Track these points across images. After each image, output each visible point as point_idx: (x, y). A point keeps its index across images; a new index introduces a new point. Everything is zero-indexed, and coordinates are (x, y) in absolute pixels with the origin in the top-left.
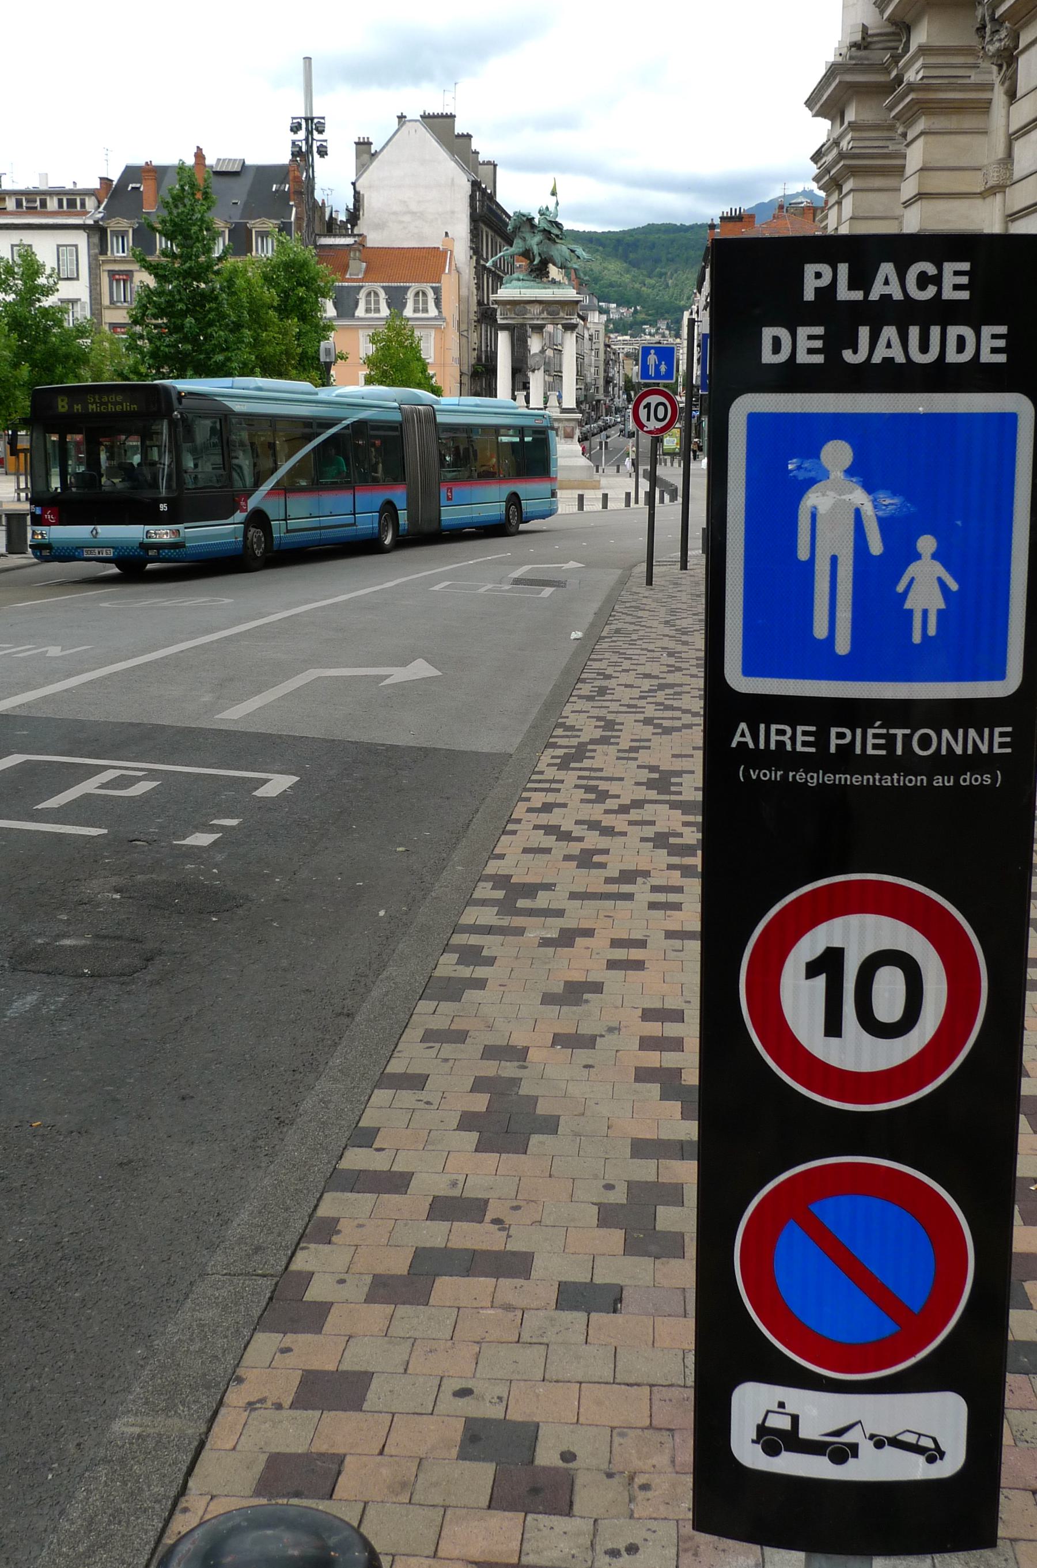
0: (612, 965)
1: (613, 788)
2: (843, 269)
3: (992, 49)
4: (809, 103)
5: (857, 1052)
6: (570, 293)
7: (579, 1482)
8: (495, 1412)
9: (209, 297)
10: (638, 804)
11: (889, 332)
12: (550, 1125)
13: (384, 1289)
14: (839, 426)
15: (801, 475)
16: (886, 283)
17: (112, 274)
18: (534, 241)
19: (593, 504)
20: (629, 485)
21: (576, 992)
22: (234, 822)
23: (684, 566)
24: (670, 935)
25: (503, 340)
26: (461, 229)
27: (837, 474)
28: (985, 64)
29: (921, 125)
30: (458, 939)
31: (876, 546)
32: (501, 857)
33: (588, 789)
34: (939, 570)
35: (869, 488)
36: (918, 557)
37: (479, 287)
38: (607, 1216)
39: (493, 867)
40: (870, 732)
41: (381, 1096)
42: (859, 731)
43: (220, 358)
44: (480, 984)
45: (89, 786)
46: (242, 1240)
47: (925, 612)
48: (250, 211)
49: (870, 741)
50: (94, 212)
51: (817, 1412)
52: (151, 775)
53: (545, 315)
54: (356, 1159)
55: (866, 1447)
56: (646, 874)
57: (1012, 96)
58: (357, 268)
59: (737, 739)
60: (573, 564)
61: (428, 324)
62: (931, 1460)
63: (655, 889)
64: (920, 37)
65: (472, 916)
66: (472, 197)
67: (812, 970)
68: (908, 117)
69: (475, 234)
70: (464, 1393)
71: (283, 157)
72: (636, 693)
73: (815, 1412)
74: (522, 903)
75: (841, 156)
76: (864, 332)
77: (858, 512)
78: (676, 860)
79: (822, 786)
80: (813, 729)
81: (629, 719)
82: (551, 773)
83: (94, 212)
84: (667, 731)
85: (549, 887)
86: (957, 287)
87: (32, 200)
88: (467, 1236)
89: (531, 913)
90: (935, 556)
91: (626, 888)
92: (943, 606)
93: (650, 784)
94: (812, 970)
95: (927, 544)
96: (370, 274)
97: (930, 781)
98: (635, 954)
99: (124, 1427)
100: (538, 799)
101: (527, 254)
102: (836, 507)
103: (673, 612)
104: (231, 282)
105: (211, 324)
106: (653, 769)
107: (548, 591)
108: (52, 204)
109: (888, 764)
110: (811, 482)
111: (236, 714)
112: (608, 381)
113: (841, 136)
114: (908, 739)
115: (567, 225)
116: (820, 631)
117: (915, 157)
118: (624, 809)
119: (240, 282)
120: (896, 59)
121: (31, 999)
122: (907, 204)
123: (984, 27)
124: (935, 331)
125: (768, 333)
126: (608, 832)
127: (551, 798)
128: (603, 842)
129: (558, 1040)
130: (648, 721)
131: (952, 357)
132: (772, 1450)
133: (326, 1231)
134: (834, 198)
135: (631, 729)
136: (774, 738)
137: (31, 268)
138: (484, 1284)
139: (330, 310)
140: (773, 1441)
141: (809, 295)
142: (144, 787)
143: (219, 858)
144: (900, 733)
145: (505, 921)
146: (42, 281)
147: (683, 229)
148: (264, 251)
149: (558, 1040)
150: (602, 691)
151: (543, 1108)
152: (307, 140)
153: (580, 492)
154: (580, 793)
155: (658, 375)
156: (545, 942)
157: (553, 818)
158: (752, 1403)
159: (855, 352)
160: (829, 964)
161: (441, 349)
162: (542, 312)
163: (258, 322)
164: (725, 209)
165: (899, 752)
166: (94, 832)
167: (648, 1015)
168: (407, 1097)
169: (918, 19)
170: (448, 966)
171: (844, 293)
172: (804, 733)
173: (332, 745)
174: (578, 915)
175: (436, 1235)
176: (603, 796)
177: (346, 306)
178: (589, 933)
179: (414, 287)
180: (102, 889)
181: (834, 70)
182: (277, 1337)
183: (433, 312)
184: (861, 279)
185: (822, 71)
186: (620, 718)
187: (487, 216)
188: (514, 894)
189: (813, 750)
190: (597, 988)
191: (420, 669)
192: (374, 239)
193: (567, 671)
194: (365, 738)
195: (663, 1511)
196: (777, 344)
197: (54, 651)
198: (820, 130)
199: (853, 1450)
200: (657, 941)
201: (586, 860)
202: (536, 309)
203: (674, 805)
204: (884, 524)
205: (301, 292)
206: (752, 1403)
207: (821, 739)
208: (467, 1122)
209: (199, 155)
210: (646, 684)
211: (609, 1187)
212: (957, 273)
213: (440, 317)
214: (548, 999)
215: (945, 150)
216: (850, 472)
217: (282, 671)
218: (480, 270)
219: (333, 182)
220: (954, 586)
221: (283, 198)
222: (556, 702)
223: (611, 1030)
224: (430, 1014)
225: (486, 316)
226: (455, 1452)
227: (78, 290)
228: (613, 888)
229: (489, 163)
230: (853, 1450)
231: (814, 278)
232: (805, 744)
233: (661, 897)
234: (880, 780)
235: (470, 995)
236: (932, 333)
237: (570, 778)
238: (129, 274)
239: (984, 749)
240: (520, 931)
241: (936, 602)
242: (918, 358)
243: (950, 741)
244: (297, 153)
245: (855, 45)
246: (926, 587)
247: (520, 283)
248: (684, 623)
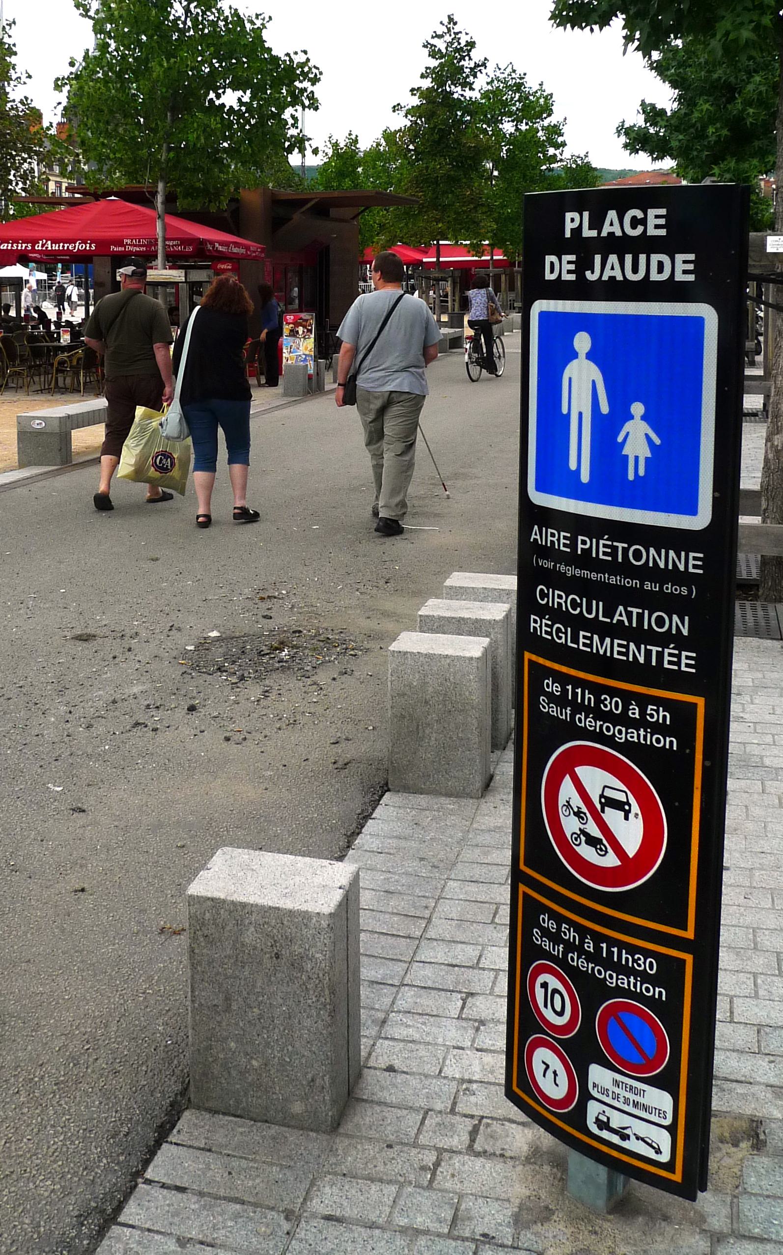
2: (586, 214)
11: (613, 259)
36: (632, 418)
40: (601, 542)
42: (594, 540)
47: (637, 458)
55: (633, 1138)
76: (598, 258)
79: (574, 576)
80: (701, 555)
86: (657, 227)
90: (643, 418)
92: (649, 455)
95: (638, 409)
97: (642, 585)
109: (612, 567)
114: (625, 551)
124: (642, 258)
131: (655, 276)
144: (620, 545)
159: (593, 273)
165: (620, 560)
171: (587, 233)
172: (695, 558)
184: (597, 223)
189: (701, 572)
196: (559, 267)
212: (657, 217)
220: (657, 441)
231: (571, 220)
232: (695, 566)
234: (609, 579)
236: (640, 261)
239: (682, 568)
241: (644, 452)
242: (631, 276)
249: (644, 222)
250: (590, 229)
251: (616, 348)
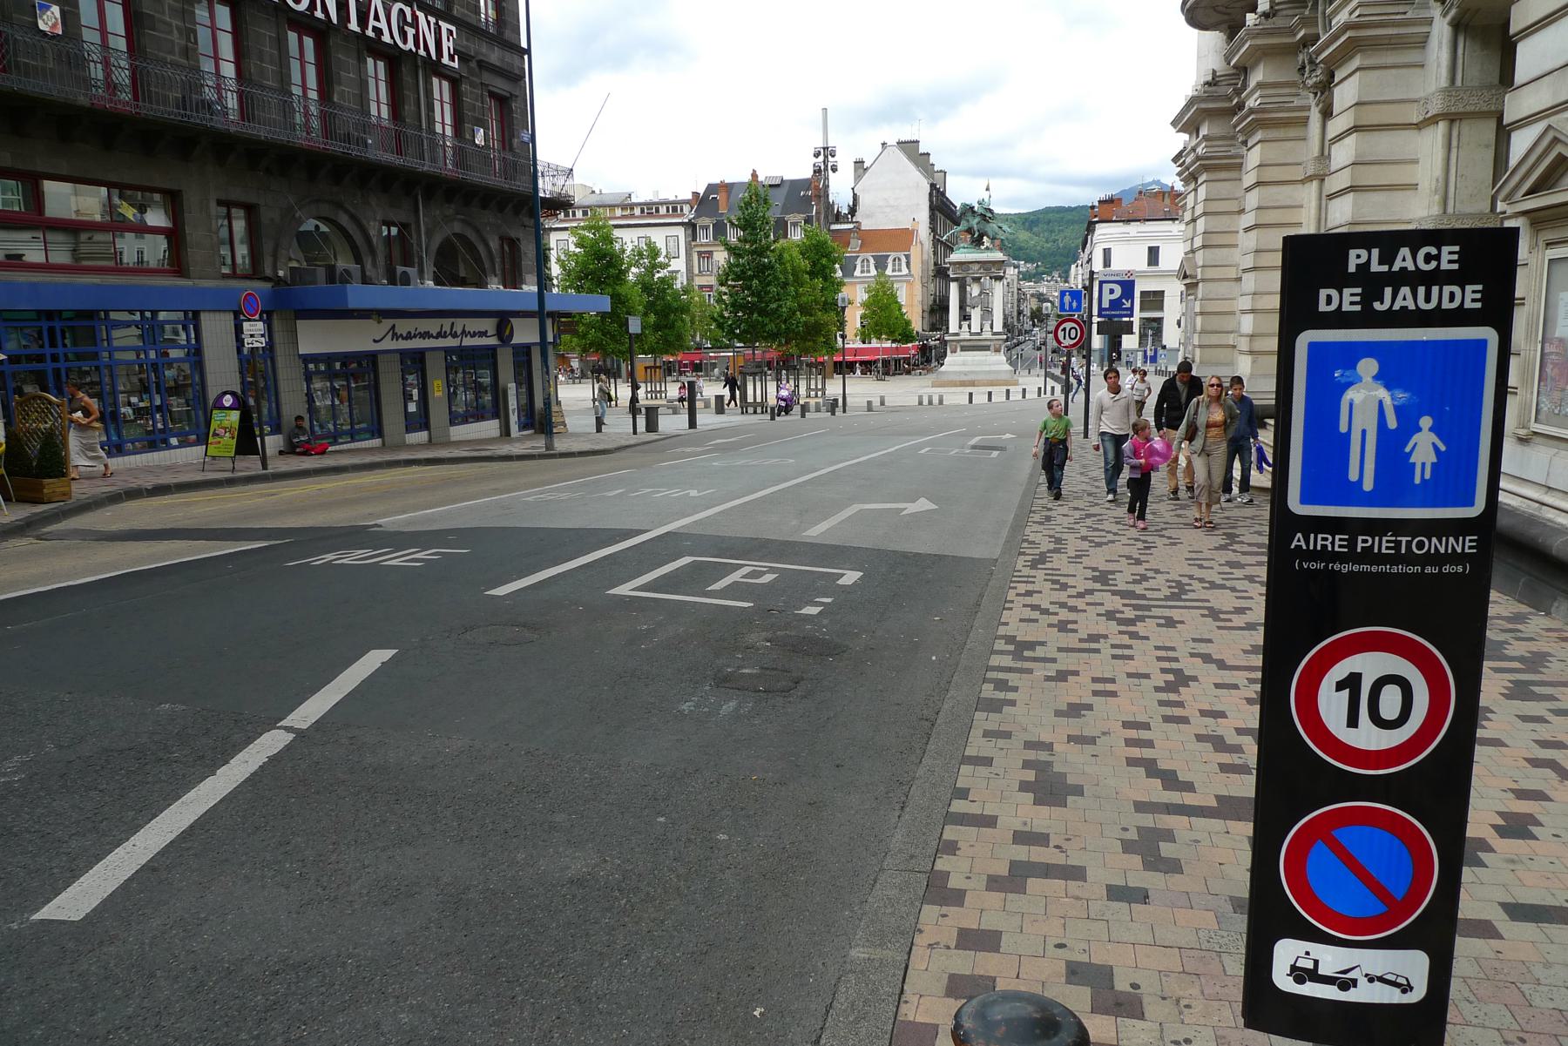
0: (1095, 693)
1: (1070, 581)
2: (1375, 252)
3: (1310, 82)
4: (1174, 123)
6: (999, 256)
7: (1145, 1001)
8: (1084, 958)
9: (770, 267)
10: (1090, 592)
12: (1078, 791)
13: (994, 883)
14: (1369, 349)
15: (1343, 380)
16: (1404, 259)
17: (700, 253)
18: (974, 222)
19: (1016, 395)
20: (1040, 382)
21: (1075, 710)
22: (829, 600)
23: (1086, 436)
24: (1130, 675)
25: (954, 287)
26: (923, 215)
27: (1368, 379)
28: (1304, 93)
29: (1259, 136)
30: (990, 675)
31: (1392, 423)
32: (1006, 624)
33: (1054, 582)
34: (1433, 438)
35: (1388, 387)
36: (1420, 430)
37: (935, 253)
38: (1128, 847)
39: (1002, 631)
41: (965, 769)
43: (774, 306)
44: (1013, 703)
45: (735, 577)
46: (900, 851)
47: (1423, 465)
48: (787, 209)
49: (1384, 545)
50: (688, 214)
51: (1331, 959)
52: (772, 570)
54: (958, 806)
55: (1362, 981)
56: (1106, 637)
57: (1327, 113)
58: (855, 243)
59: (1295, 543)
60: (1008, 436)
61: (901, 279)
62: (1404, 991)
63: (1113, 646)
64: (1257, 77)
65: (995, 660)
66: (931, 194)
67: (1340, 686)
68: (1249, 131)
69: (933, 219)
70: (1061, 946)
71: (807, 173)
72: (1071, 520)
73: (1329, 958)
74: (1026, 653)
75: (1198, 158)
76: (1388, 291)
77: (1381, 402)
78: (1123, 628)
81: (1070, 537)
82: (1026, 571)
83: (688, 214)
84: (1099, 545)
85: (1042, 644)
86: (1450, 262)
87: (650, 208)
88: (1038, 854)
89: (1035, 659)
90: (1431, 429)
91: (1094, 646)
93: (1095, 579)
94: (1340, 686)
95: (1426, 422)
96: (863, 248)
98: (1109, 687)
99: (858, 953)
100: (1022, 588)
101: (970, 231)
102: (1366, 400)
103: (1084, 466)
104: (780, 257)
105: (769, 284)
106: (1094, 569)
107: (995, 454)
108: (663, 210)
110: (1349, 385)
111: (816, 532)
112: (1020, 313)
113: (1198, 145)
114: (1409, 543)
115: (997, 210)
116: (1353, 476)
117: (1253, 157)
118: (1080, 595)
119: (786, 256)
120: (1238, 92)
121: (733, 704)
122: (1248, 190)
123: (1303, 67)
124: (1435, 289)
125: (1323, 293)
126: (1073, 609)
127: (1030, 587)
128: (1072, 616)
129: (1070, 738)
130: (1084, 538)
131: (1446, 305)
132: (1299, 980)
133: (952, 848)
134: (1192, 186)
135: (1073, 544)
136: (1320, 543)
137: (654, 252)
138: (1058, 884)
139: (839, 274)
140: (1299, 975)
141: (1352, 269)
142: (767, 578)
143: (825, 622)
144: (1404, 539)
145: (1019, 665)
146: (661, 259)
147: (1070, 209)
148: (796, 235)
149: (1070, 738)
150: (1048, 519)
151: (1070, 780)
153: (990, 389)
154: (1049, 585)
155: (1071, 309)
156: (1048, 679)
157: (1034, 600)
158: (1287, 952)
160: (1351, 683)
161: (911, 296)
163: (798, 282)
164: (1102, 196)
166: (746, 605)
167: (1126, 725)
168: (982, 771)
169: (1255, 65)
170: (988, 691)
173: (880, 554)
174: (1066, 662)
175: (1022, 853)
176: (1064, 587)
177: (849, 270)
178: (1076, 673)
179: (893, 255)
180: (757, 638)
181: (1192, 102)
182: (936, 908)
183: (905, 271)
184: (1387, 258)
185: (1183, 103)
186: (1064, 536)
187: (940, 207)
188: (1021, 648)
190: (1089, 707)
191: (923, 505)
192: (866, 225)
193: (1021, 506)
194: (898, 548)
195: (1202, 1021)
196: (1328, 299)
197: (693, 493)
198: (1180, 140)
199: (1354, 982)
200: (1122, 679)
201: (1063, 627)
202: (976, 267)
203: (1114, 593)
204: (1397, 409)
205: (824, 261)
206: (1287, 952)
207: (1352, 544)
208: (1024, 787)
209: (754, 175)
210: (1077, 514)
211: (1125, 829)
213: (910, 275)
214: (1058, 713)
215: (1276, 152)
216: (1376, 378)
217: (841, 507)
218: (936, 242)
219: (840, 189)
220: (1443, 448)
221: (808, 199)
222: (1019, 525)
223: (1104, 734)
224: (984, 720)
225: (941, 273)
226: (1063, 979)
227: (679, 265)
228: (1086, 645)
230: (1354, 982)
231: (1355, 258)
233: (1119, 652)
235: (1006, 709)
237: (1040, 574)
238: (710, 253)
240: (1030, 671)
242: (1423, 306)
243: (1435, 544)
244: (817, 171)
245: (1207, 83)
246: (1424, 448)
248: (1094, 474)
249: (1438, 258)
250: (1380, 263)
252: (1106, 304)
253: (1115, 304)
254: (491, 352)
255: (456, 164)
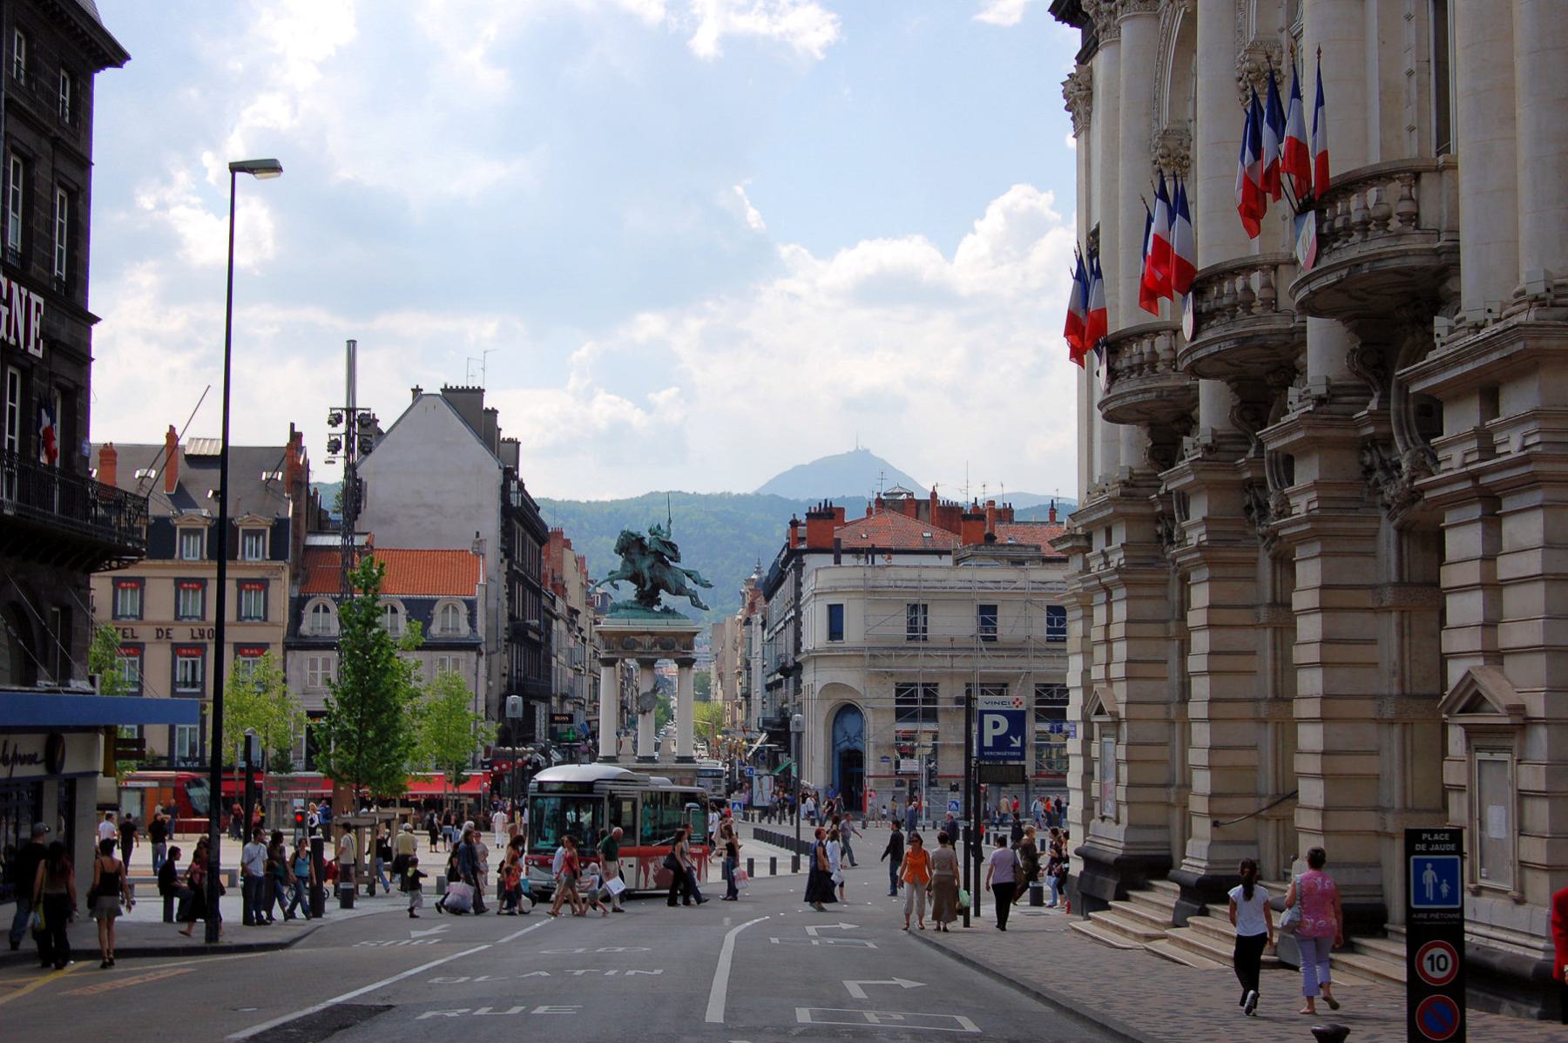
5: (1437, 974)
16: (1436, 837)
26: (491, 526)
37: (511, 597)
53: (658, 648)
69: (507, 533)
102: (1429, 876)
152: (347, 434)
160: (1431, 958)
162: (654, 645)
196: (1418, 847)
209: (172, 435)
229: (510, 441)
231: (1424, 836)
246: (1445, 888)
247: (628, 612)
251: (1437, 866)
252: (988, 742)
253: (1001, 742)
254: (37, 785)
255: (62, 511)
